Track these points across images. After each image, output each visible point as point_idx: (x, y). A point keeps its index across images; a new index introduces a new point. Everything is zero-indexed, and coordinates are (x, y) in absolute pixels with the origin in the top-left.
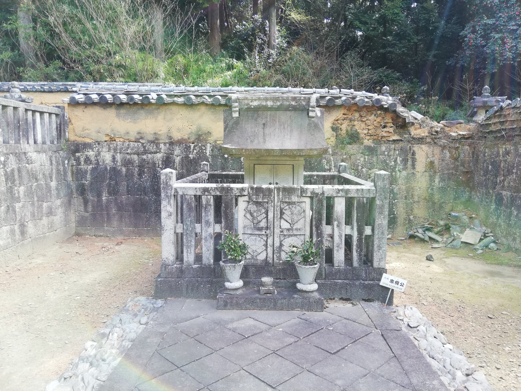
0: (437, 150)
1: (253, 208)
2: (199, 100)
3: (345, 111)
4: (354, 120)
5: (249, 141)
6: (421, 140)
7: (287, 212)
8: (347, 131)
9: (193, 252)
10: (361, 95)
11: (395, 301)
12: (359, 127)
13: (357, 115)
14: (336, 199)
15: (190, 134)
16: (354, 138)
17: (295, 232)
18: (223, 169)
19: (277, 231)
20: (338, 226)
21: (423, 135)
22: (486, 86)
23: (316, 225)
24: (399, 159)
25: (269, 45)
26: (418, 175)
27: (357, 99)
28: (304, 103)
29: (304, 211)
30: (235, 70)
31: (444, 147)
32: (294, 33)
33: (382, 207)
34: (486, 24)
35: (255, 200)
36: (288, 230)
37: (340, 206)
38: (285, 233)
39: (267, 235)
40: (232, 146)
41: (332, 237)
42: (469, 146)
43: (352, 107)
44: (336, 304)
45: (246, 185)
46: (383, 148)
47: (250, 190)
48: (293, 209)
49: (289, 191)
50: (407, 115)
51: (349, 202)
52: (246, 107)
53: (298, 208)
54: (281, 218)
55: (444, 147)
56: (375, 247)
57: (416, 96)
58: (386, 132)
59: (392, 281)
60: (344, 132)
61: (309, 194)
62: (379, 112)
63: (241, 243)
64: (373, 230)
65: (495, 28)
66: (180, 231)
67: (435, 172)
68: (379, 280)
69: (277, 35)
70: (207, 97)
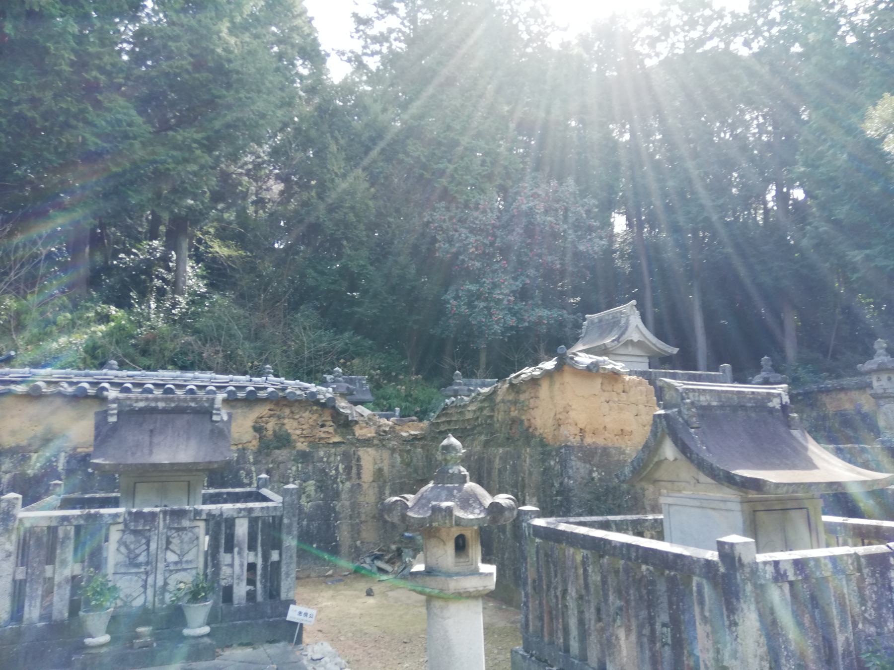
0: (386, 454)
1: (129, 538)
2: (52, 389)
3: (272, 407)
4: (284, 418)
5: (129, 453)
6: (367, 442)
7: (175, 541)
8: (274, 431)
9: (38, 604)
10: (293, 386)
11: (305, 638)
12: (291, 426)
13: (287, 411)
14: (237, 521)
15: (32, 438)
16: (283, 440)
17: (185, 566)
18: (86, 491)
19: (161, 566)
20: (239, 553)
21: (369, 435)
22: (457, 372)
23: (213, 554)
24: (341, 467)
25: (176, 286)
26: (365, 486)
27: (288, 391)
28: (206, 405)
29: (197, 538)
30: (113, 324)
31: (393, 450)
32: (217, 274)
33: (290, 526)
34: (469, 291)
35: (132, 528)
36: (176, 563)
37: (242, 529)
38: (172, 568)
39: (147, 573)
40: (105, 460)
41: (232, 565)
42: (422, 448)
43: (280, 400)
44: (234, 651)
45: (121, 510)
46: (322, 453)
47: (126, 516)
48: (183, 536)
49: (179, 514)
50: (348, 412)
51: (253, 522)
52: (128, 409)
53: (190, 534)
54: (167, 548)
55: (393, 450)
56: (283, 574)
57: (394, 374)
58: (324, 432)
59: (300, 613)
60: (270, 432)
61: (204, 517)
62: (315, 408)
63: (110, 584)
64: (280, 555)
65: (479, 296)
66: (20, 576)
67: (385, 482)
68: (286, 615)
69: (192, 276)
70: (65, 385)
